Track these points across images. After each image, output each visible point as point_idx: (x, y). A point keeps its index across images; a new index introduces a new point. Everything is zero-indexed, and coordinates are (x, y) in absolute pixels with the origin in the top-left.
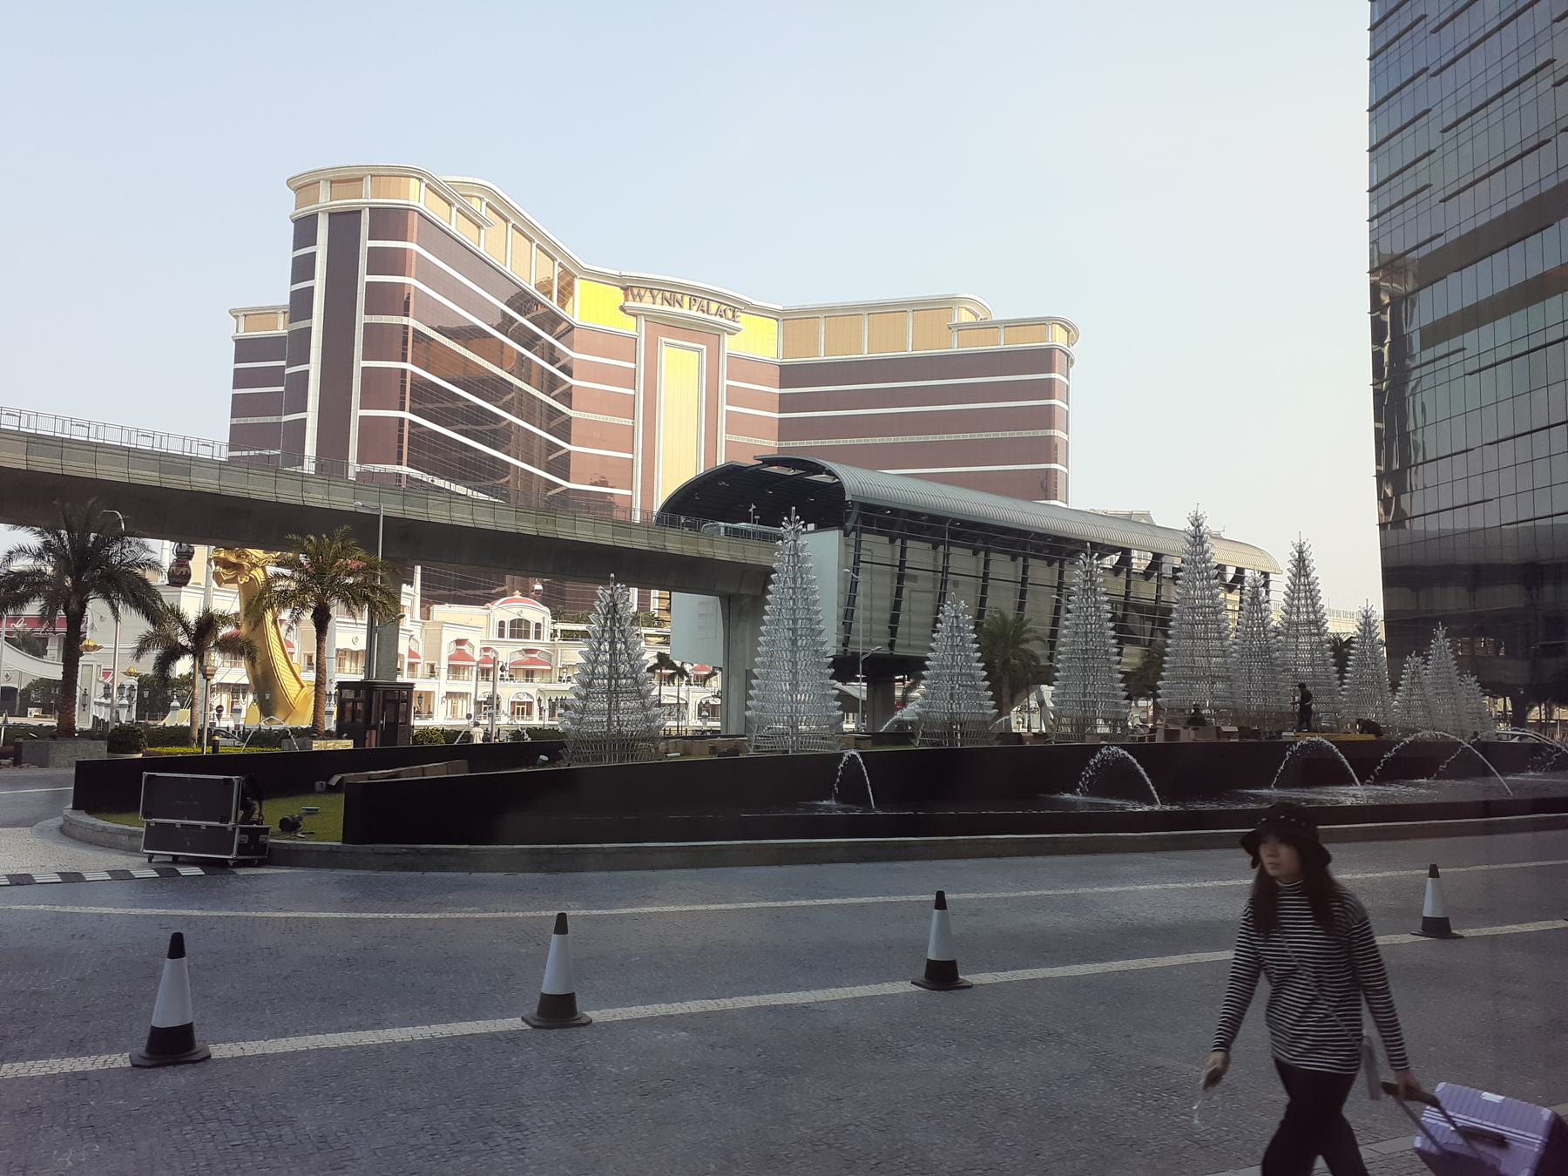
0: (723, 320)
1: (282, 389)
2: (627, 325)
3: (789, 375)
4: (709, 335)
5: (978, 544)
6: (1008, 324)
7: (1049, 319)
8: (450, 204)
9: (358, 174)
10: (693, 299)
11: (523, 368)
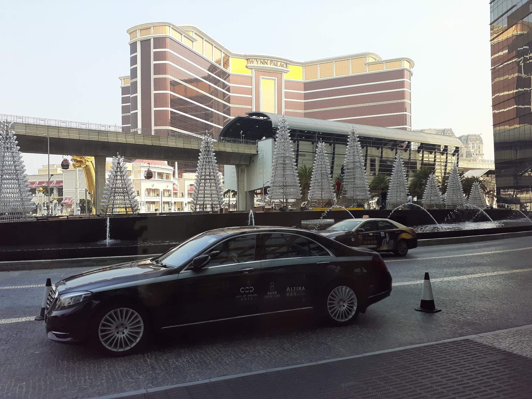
0: (283, 68)
1: (130, 104)
2: (248, 73)
3: (307, 86)
4: (277, 74)
5: (332, 141)
6: (387, 62)
7: (402, 58)
8: (181, 34)
11: (215, 93)
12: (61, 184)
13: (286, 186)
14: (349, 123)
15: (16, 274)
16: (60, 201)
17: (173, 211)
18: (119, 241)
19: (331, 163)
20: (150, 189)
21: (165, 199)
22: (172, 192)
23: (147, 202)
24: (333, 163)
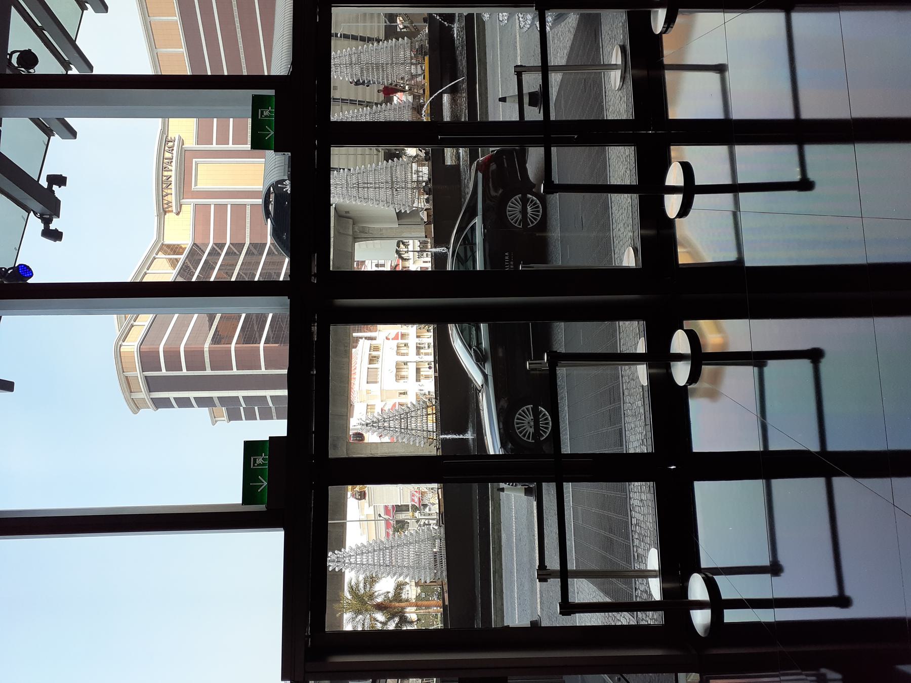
0: (175, 148)
1: (256, 408)
2: (188, 210)
4: (186, 158)
8: (132, 326)
9: (124, 380)
10: (164, 169)
12: (390, 508)
13: (392, 182)
14: (271, 46)
15: (504, 536)
16: (415, 509)
17: (431, 340)
18: (470, 425)
19: (352, 107)
20: (396, 375)
21: (412, 349)
22: (400, 341)
23: (418, 380)
24: (352, 102)
